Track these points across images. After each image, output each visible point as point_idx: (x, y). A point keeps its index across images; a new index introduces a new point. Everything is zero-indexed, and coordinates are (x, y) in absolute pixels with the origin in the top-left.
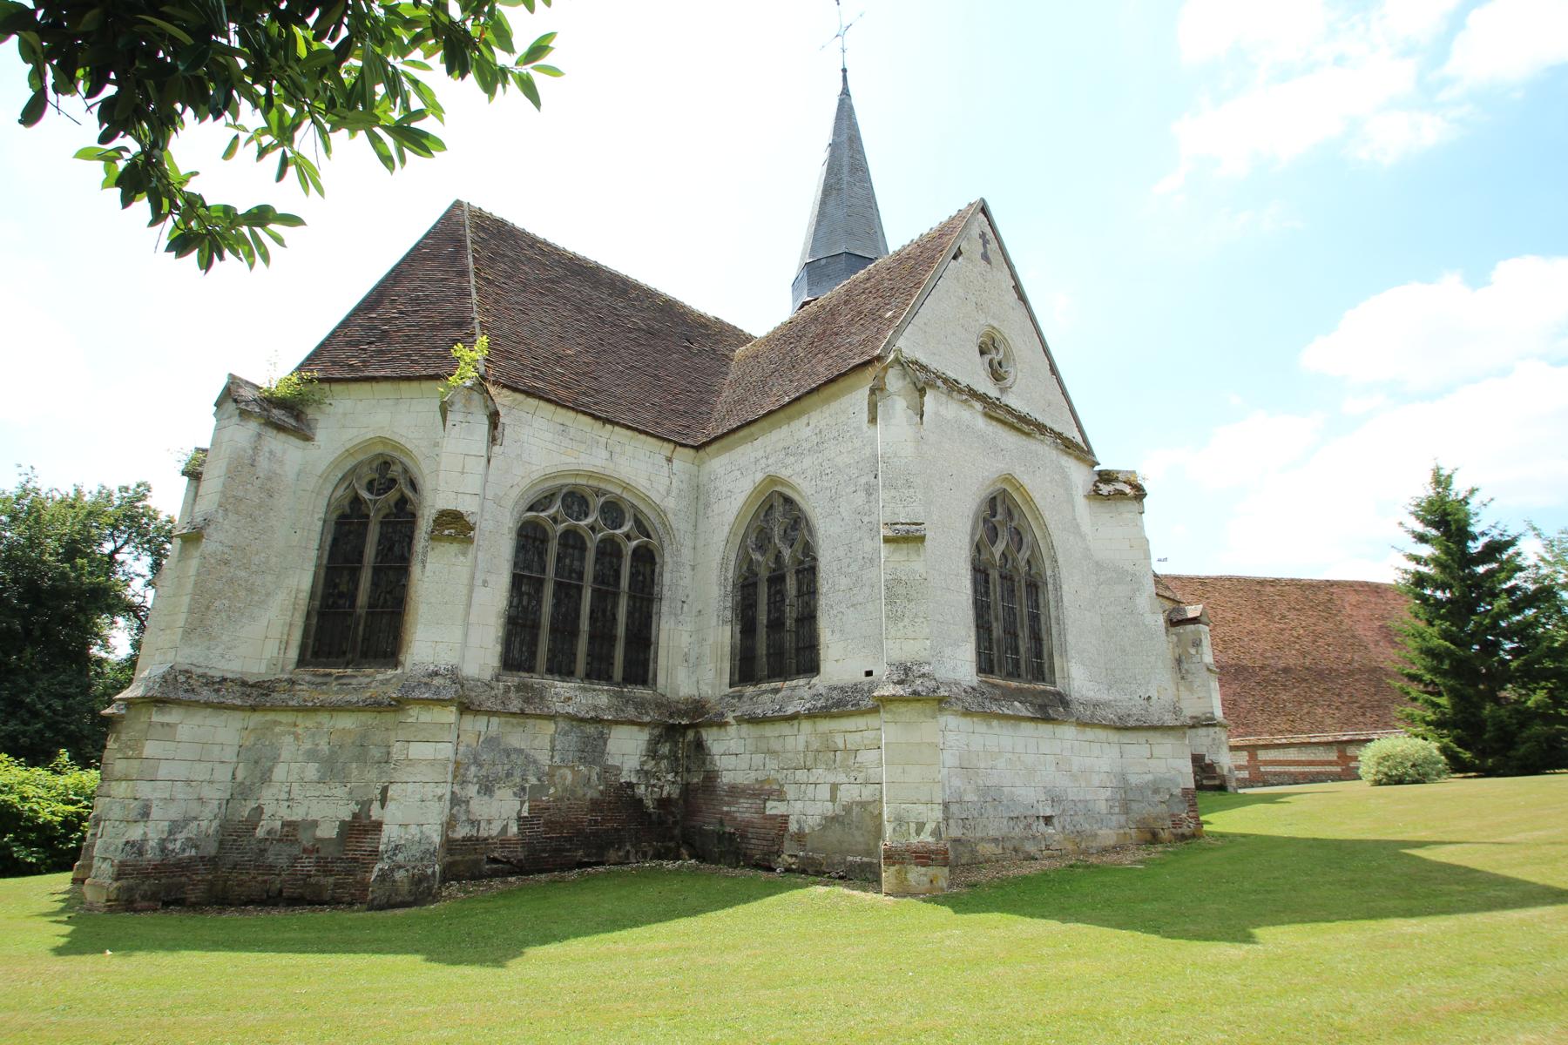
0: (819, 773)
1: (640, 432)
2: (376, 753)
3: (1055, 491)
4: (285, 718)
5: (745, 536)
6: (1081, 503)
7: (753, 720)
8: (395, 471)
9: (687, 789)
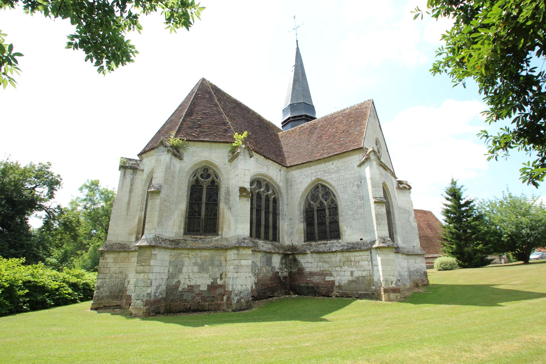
0: (345, 268)
1: (275, 162)
2: (217, 263)
3: (392, 186)
4: (185, 252)
5: (307, 196)
6: (395, 189)
7: (319, 252)
8: (210, 171)
9: (290, 273)
